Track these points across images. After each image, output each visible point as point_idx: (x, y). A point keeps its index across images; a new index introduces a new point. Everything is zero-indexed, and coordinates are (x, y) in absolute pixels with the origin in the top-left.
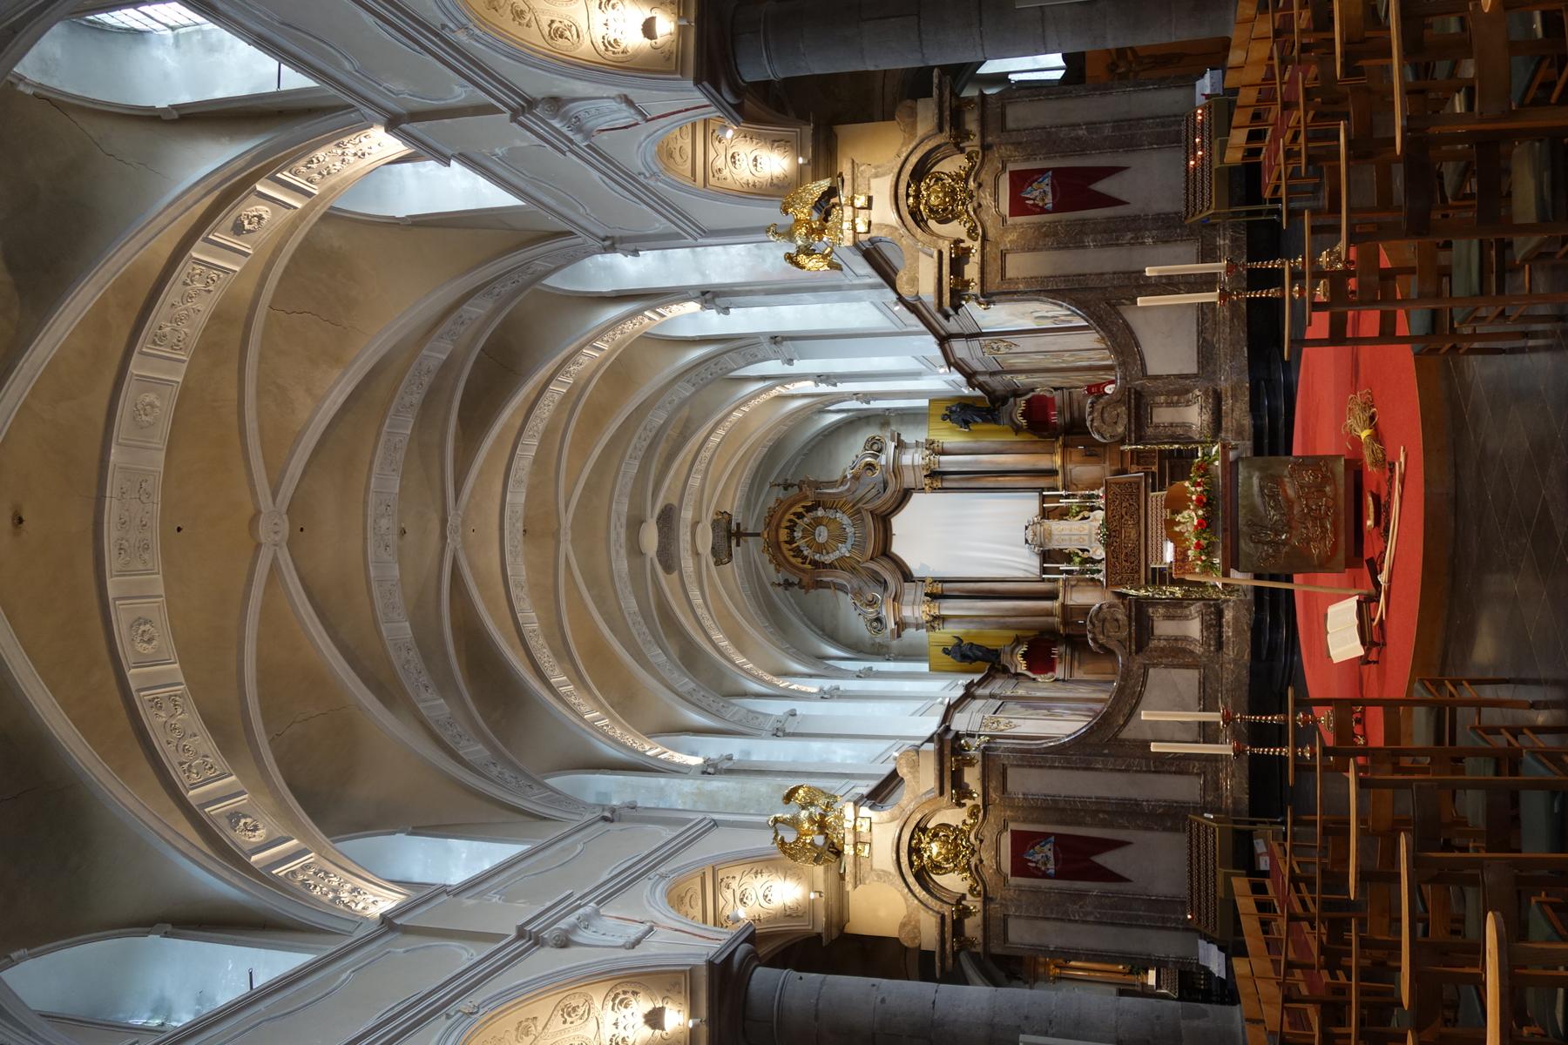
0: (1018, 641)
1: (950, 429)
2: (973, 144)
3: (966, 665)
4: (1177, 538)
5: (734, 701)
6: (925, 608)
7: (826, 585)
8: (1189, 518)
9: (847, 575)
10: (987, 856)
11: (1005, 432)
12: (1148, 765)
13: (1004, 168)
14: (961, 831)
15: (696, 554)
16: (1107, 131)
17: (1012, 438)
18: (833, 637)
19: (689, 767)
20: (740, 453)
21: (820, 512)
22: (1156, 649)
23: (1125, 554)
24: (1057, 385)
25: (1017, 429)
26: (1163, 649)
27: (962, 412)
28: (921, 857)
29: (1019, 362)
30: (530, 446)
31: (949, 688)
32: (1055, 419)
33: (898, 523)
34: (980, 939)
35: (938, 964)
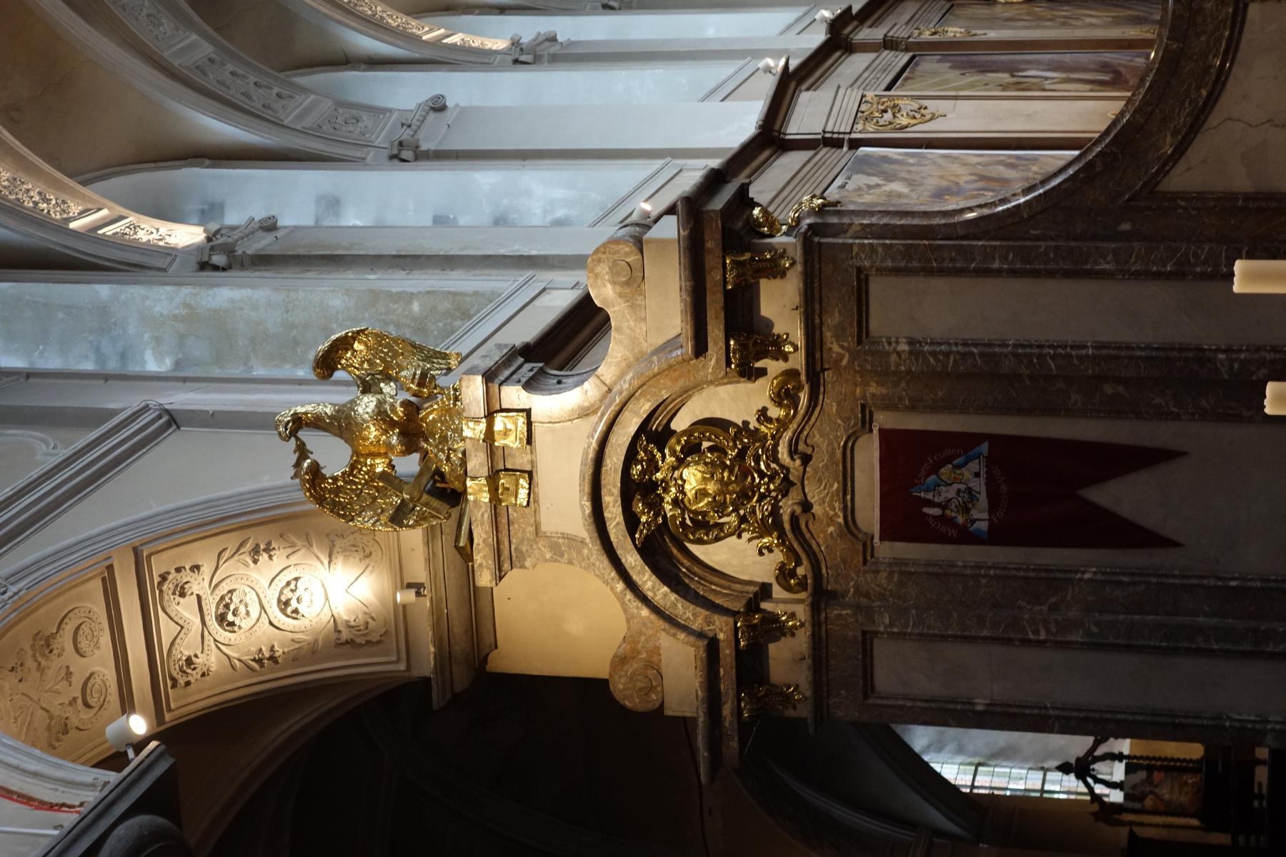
10: (821, 495)
19: (171, 253)
28: (655, 505)
35: (703, 753)
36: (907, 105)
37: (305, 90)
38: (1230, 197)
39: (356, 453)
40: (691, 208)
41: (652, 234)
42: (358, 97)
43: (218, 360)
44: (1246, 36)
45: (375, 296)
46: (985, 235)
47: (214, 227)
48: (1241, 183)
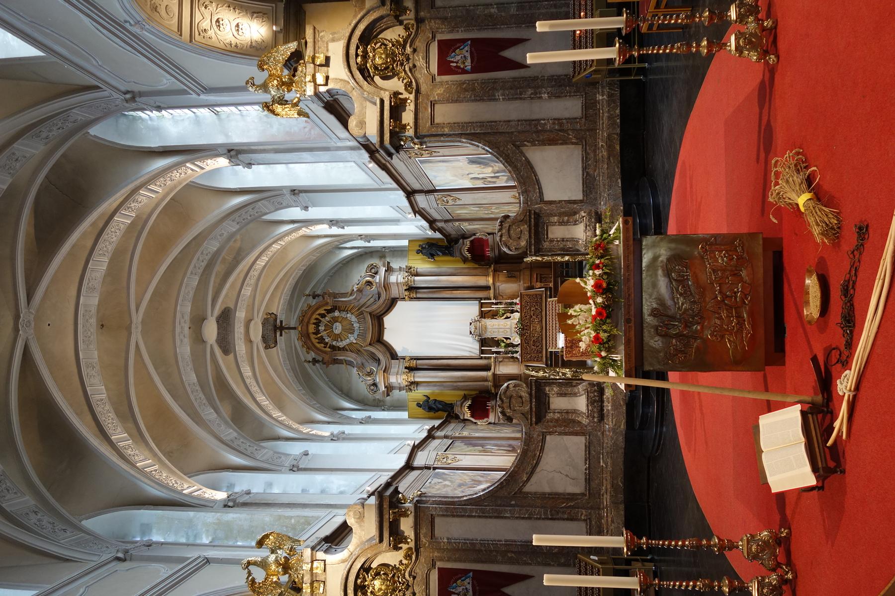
0: (465, 398)
1: (422, 259)
2: (409, 17)
3: (432, 414)
5: (264, 444)
6: (404, 377)
7: (340, 362)
9: (354, 355)
12: (546, 513)
13: (434, 37)
15: (249, 341)
16: (513, 10)
17: (462, 265)
18: (348, 395)
19: (215, 501)
20: (282, 274)
21: (337, 314)
22: (551, 420)
23: (532, 343)
24: (490, 231)
25: (465, 260)
26: (557, 420)
27: (429, 249)
30: (100, 265)
31: (417, 431)
33: (388, 320)
36: (451, 457)
37: (264, 448)
38: (544, 494)
39: (267, 574)
40: (379, 493)
41: (367, 502)
42: (282, 450)
43: (227, 538)
44: (546, 445)
45: (280, 517)
46: (471, 504)
47: (230, 493)
48: (547, 490)
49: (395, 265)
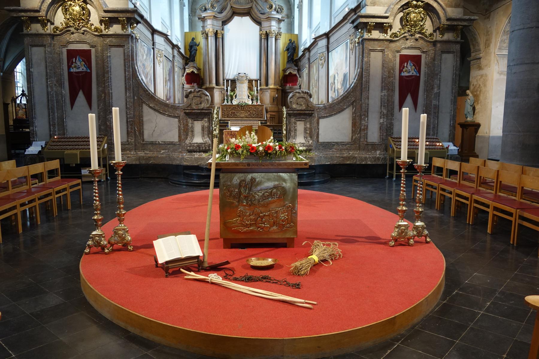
0: (199, 69)
2: (438, 37)
3: (188, 47)
4: (242, 132)
6: (211, 30)
8: (252, 139)
11: (284, 66)
12: (130, 118)
13: (423, 52)
14: (87, 23)
16: (434, 102)
17: (281, 69)
23: (233, 112)
25: (284, 71)
26: (187, 125)
27: (292, 48)
29: (314, 69)
31: (177, 38)
32: (288, 86)
33: (247, 20)
34: (30, 32)
49: (282, 25)
